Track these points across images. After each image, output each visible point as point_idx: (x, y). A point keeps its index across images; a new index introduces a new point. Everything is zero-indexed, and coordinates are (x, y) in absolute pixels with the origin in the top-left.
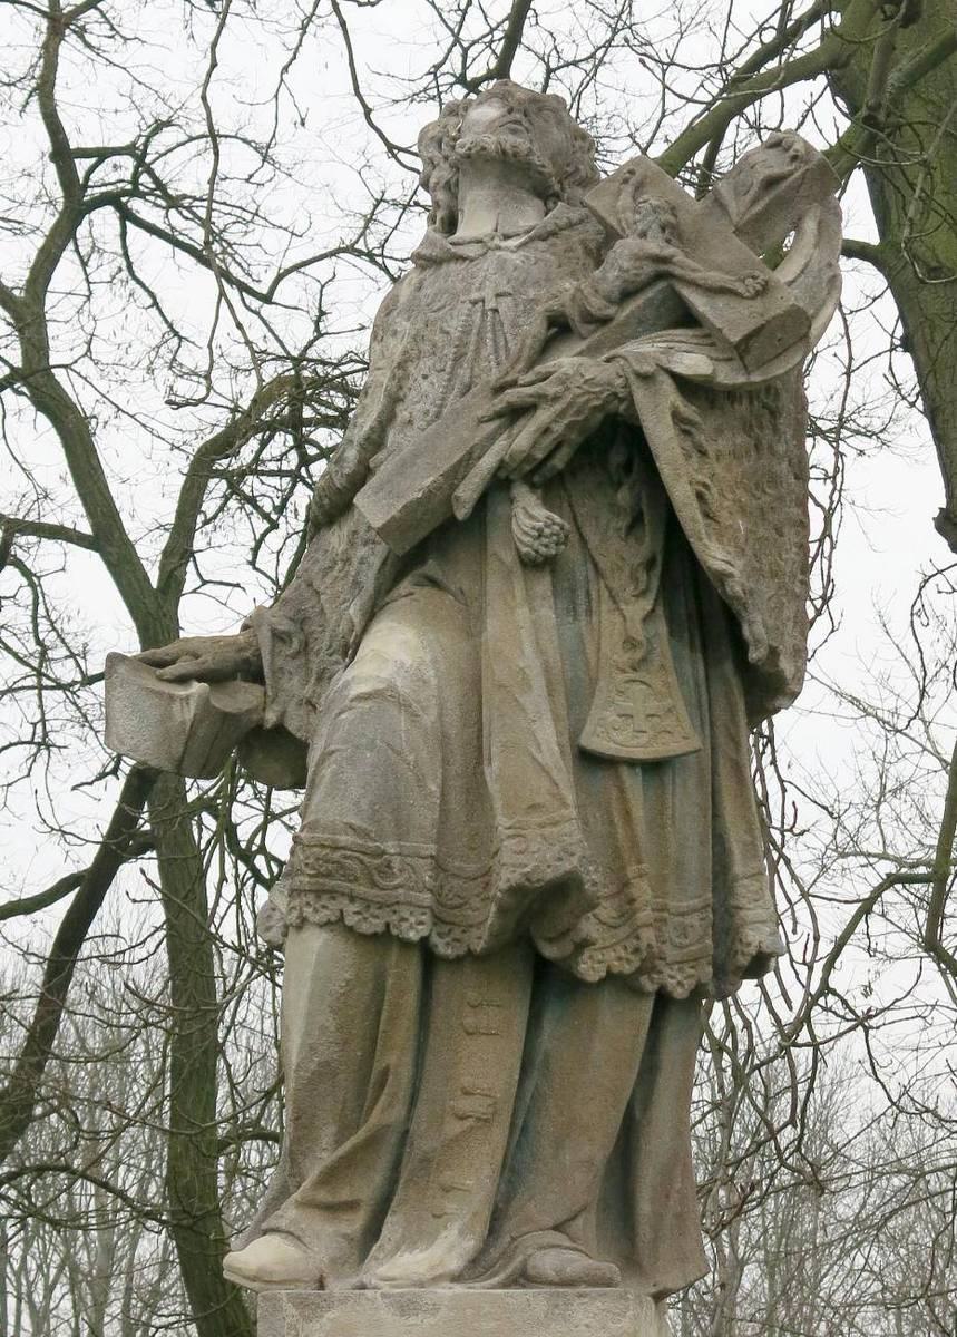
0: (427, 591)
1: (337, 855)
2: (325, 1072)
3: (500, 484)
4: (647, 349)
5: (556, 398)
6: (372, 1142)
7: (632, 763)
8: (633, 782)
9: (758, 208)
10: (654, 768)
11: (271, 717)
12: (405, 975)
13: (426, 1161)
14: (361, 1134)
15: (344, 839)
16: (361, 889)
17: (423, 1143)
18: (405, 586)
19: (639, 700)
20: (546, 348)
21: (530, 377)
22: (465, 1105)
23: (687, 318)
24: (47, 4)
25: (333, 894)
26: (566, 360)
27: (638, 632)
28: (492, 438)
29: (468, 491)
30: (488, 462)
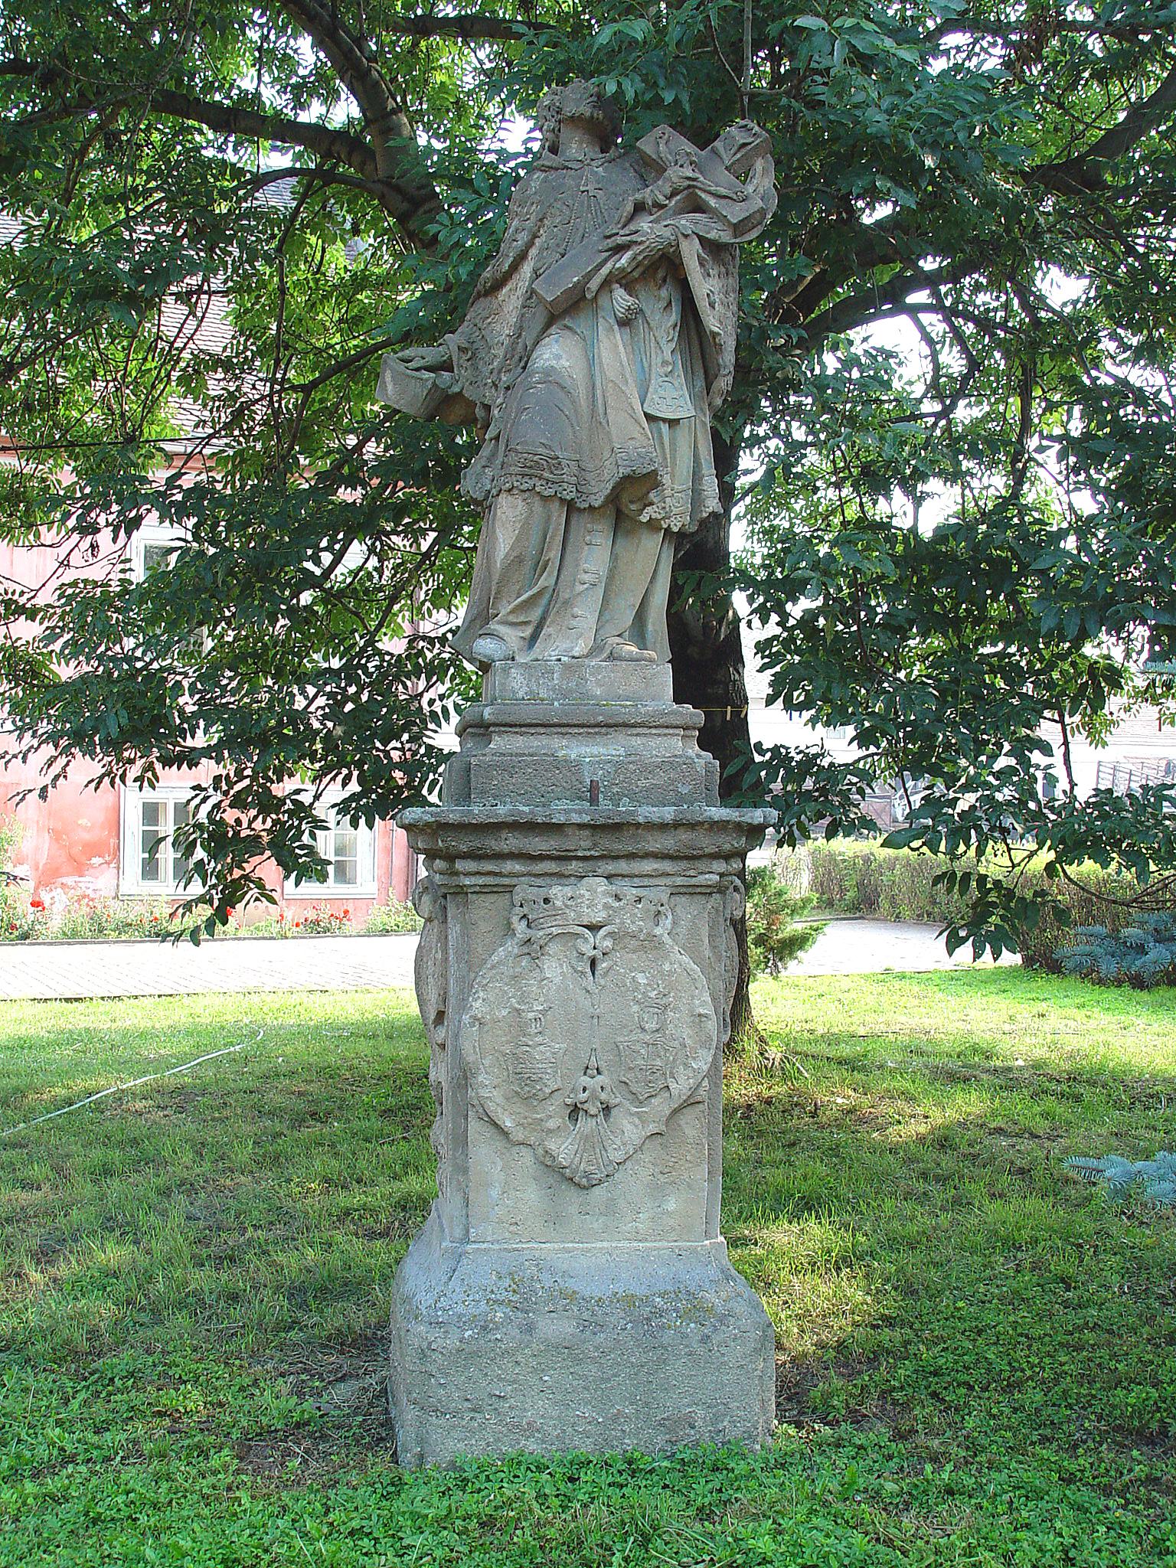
0: (568, 333)
1: (536, 458)
2: (519, 560)
3: (606, 283)
4: (685, 222)
5: (642, 242)
6: (540, 593)
7: (664, 420)
8: (664, 427)
9: (738, 156)
10: (673, 423)
11: (456, 389)
12: (559, 516)
13: (566, 602)
14: (535, 590)
15: (540, 450)
16: (546, 475)
17: (565, 595)
18: (553, 329)
19: (670, 392)
20: (631, 218)
21: (622, 232)
22: (586, 577)
23: (699, 207)
24: (5, 218)
25: (531, 476)
26: (644, 224)
27: (668, 357)
28: (606, 261)
29: (594, 284)
30: (605, 271)
